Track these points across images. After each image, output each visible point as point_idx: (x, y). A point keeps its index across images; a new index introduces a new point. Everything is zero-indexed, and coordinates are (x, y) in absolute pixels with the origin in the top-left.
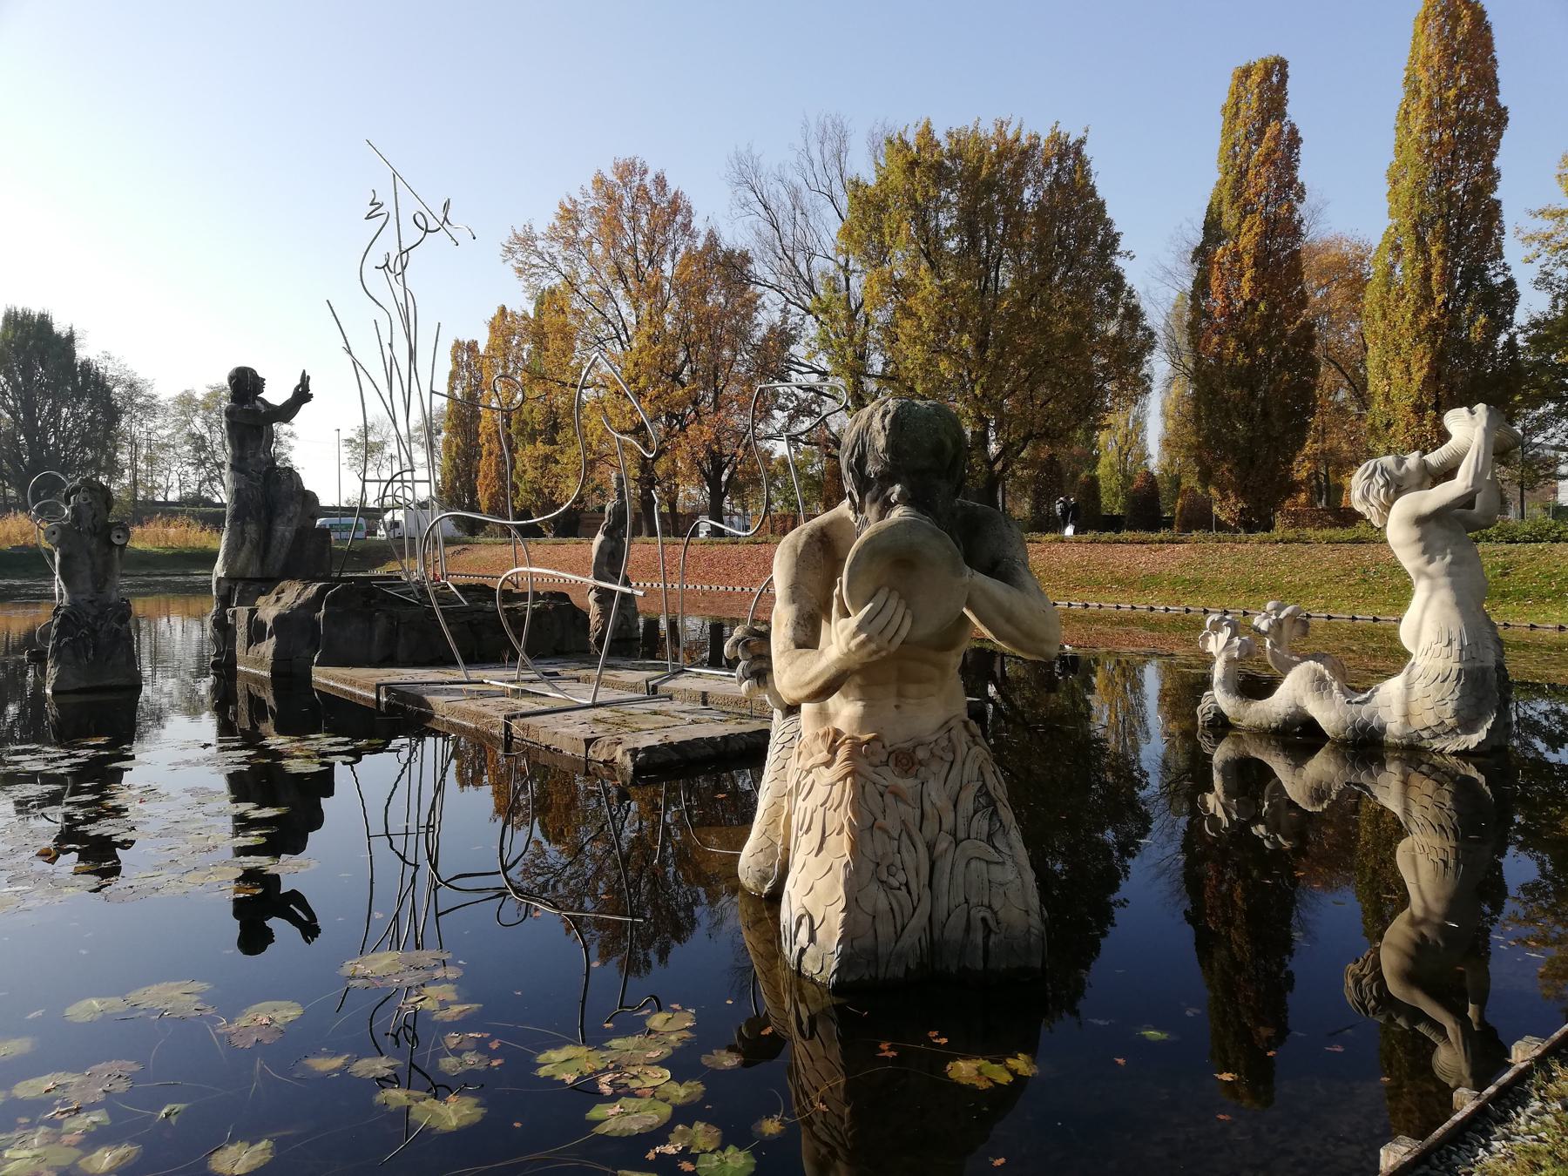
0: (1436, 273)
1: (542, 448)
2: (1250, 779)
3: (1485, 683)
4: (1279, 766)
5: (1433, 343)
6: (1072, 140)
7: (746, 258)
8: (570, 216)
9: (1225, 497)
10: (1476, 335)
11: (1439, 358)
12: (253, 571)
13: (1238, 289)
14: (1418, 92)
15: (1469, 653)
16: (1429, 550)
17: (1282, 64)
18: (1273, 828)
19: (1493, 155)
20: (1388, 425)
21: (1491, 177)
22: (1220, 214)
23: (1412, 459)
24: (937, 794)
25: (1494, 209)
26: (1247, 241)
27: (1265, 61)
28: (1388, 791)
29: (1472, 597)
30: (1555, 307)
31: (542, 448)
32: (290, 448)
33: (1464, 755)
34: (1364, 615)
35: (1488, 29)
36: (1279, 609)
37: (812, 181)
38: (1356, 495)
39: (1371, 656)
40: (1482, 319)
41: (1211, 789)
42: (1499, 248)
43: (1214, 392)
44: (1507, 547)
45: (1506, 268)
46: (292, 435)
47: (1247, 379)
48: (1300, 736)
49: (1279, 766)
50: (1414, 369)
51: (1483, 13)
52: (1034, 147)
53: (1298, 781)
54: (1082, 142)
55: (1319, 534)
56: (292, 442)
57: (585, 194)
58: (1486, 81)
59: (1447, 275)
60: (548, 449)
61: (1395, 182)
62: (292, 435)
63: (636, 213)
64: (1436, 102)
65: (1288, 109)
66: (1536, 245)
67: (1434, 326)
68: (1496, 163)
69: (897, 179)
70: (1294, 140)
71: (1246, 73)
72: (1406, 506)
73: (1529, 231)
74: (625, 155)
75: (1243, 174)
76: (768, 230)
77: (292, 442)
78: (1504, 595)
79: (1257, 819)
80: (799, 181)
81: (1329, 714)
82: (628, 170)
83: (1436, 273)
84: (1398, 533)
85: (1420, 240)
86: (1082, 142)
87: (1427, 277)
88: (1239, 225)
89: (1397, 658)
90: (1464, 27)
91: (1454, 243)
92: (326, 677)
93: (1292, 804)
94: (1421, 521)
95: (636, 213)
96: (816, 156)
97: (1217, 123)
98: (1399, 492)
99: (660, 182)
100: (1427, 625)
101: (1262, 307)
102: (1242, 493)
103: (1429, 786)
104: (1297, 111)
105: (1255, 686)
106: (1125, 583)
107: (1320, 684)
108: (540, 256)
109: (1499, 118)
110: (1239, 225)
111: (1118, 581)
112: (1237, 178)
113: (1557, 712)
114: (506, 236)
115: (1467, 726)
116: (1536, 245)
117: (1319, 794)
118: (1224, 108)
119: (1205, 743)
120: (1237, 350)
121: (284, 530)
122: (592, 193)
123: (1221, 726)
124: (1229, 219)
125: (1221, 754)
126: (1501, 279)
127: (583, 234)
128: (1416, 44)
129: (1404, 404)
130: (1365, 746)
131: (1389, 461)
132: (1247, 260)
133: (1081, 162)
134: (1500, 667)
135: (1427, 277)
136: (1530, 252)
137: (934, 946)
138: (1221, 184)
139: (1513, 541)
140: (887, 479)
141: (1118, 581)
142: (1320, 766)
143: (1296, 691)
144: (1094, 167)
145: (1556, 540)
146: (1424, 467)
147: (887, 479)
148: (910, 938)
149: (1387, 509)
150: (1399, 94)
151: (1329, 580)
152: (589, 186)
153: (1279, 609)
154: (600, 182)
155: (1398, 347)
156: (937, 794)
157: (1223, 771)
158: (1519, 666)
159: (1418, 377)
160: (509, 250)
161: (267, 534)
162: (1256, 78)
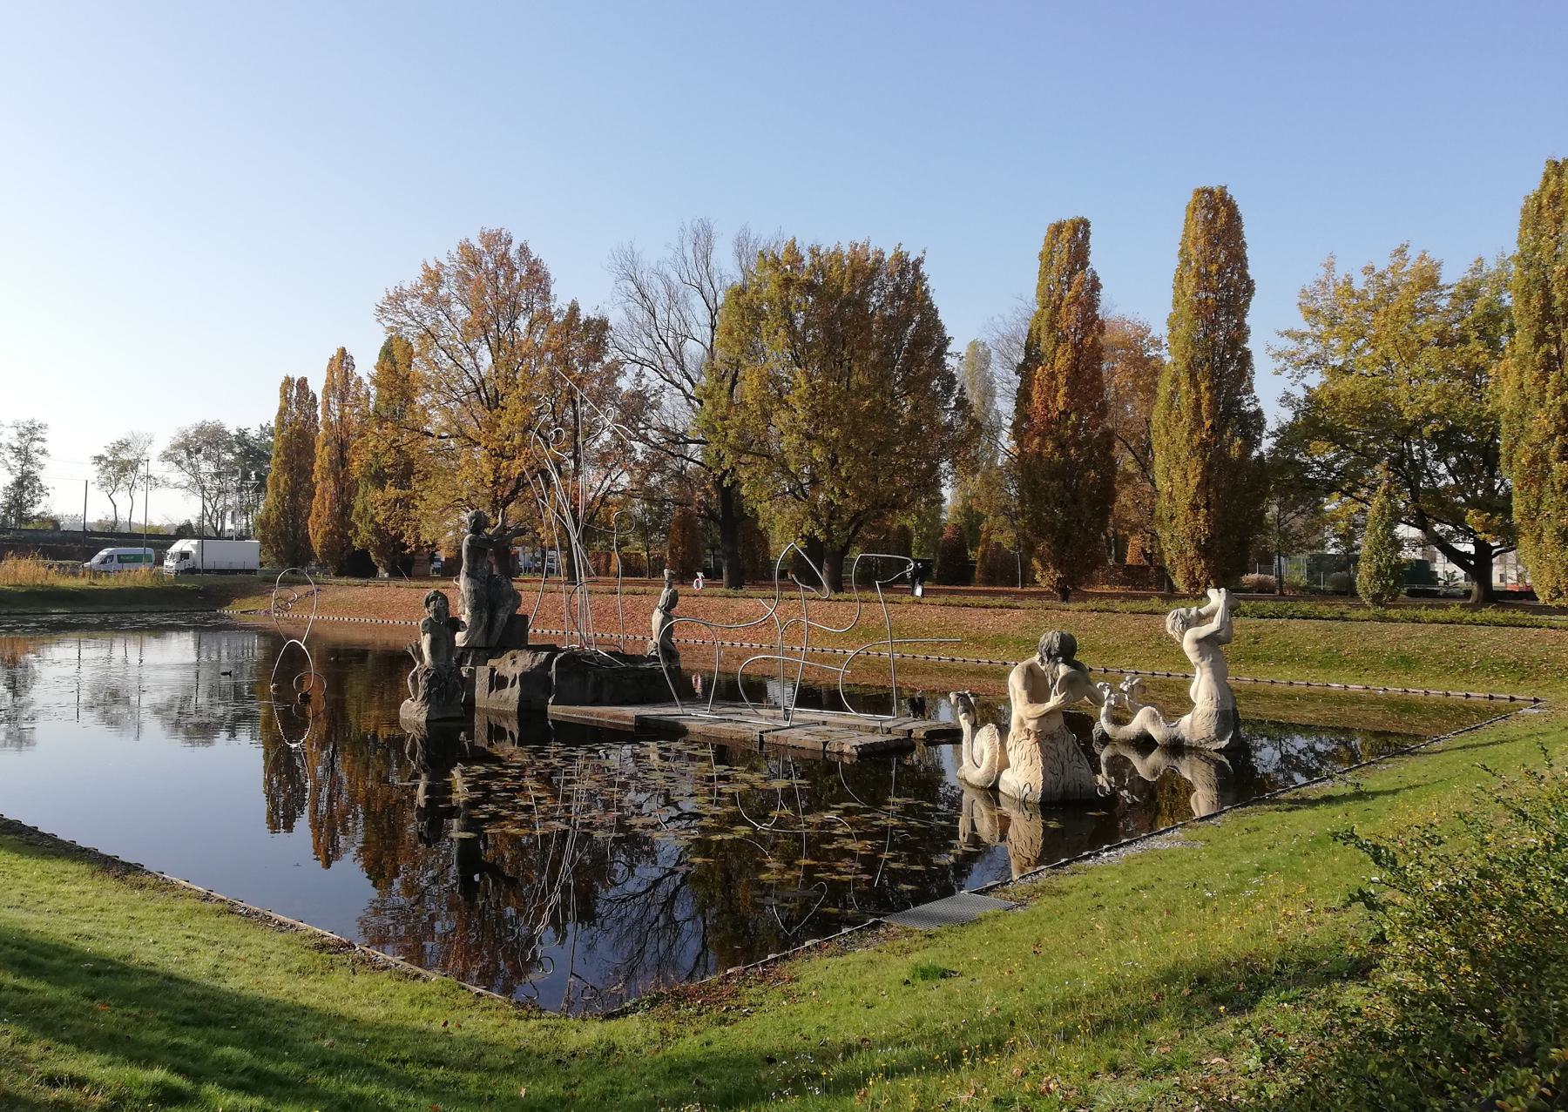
0: (1205, 403)
1: (392, 492)
2: (1119, 766)
3: (1227, 718)
4: (1135, 759)
5: (1204, 457)
6: (912, 258)
7: (600, 327)
8: (434, 277)
9: (1045, 567)
10: (1235, 453)
11: (1208, 468)
12: (482, 643)
13: (1054, 401)
14: (1188, 262)
15: (1220, 703)
16: (1202, 655)
17: (1086, 224)
18: (1132, 792)
19: (1244, 315)
20: (1172, 518)
21: (1242, 332)
22: (1039, 339)
23: (1194, 611)
24: (1062, 748)
25: (1245, 359)
26: (1061, 363)
27: (1072, 222)
28: (1188, 770)
29: (1219, 677)
30: (1296, 418)
31: (392, 492)
32: (41, 467)
33: (1219, 751)
34: (1161, 671)
35: (1239, 218)
36: (1132, 679)
37: (686, 278)
38: (1169, 626)
39: (1175, 702)
40: (1239, 441)
41: (1100, 772)
42: (1251, 385)
43: (1035, 482)
44: (1258, 621)
45: (1257, 400)
46: (44, 452)
47: (1063, 472)
48: (1144, 744)
49: (1135, 759)
50: (1190, 476)
51: (1235, 207)
52: (878, 261)
53: (1144, 766)
54: (919, 261)
55: (1124, 607)
56: (42, 459)
57: (451, 259)
58: (1238, 258)
59: (1213, 403)
60: (401, 493)
61: (1173, 329)
62: (44, 452)
63: (500, 282)
64: (1203, 270)
65: (1090, 259)
66: (1283, 361)
67: (1204, 445)
68: (1247, 321)
69: (771, 289)
70: (1095, 285)
71: (1058, 229)
72: (1191, 634)
73: (1277, 349)
74: (493, 226)
75: (1057, 308)
76: (642, 315)
77: (42, 459)
78: (1255, 658)
79: (1123, 788)
80: (674, 277)
81: (1158, 733)
82: (494, 239)
83: (1205, 403)
84: (1188, 646)
85: (1193, 376)
86: (919, 261)
87: (1198, 405)
88: (1055, 350)
89: (1187, 705)
90: (1221, 221)
91: (1217, 374)
92: (555, 710)
93: (1140, 779)
94: (1198, 641)
95: (500, 282)
96: (689, 254)
97: (1035, 266)
98: (1189, 627)
99: (524, 250)
100: (1202, 689)
101: (1073, 417)
102: (1059, 565)
103: (1205, 765)
104: (1098, 260)
105: (1119, 720)
106: (978, 641)
107: (1154, 717)
108: (409, 314)
109: (1250, 288)
110: (1055, 350)
111: (973, 639)
112: (1052, 305)
113: (1312, 749)
114: (380, 297)
115: (1220, 737)
116: (1283, 361)
117: (1154, 772)
118: (1041, 255)
119: (1097, 750)
120: (1055, 449)
121: (502, 616)
122: (457, 257)
123: (1105, 739)
124: (1046, 345)
125: (1104, 754)
126: (1252, 408)
127: (443, 292)
128: (1187, 228)
129: (1183, 503)
130: (1176, 748)
131: (1183, 610)
132: (1061, 379)
133: (919, 277)
134: (1235, 710)
135: (1198, 405)
136: (1279, 365)
137: (1065, 793)
138: (1039, 316)
139: (1262, 617)
140: (1057, 655)
141: (973, 639)
142: (1155, 758)
143: (1141, 721)
144: (931, 283)
145: (1292, 617)
146: (1199, 614)
147: (1057, 655)
148: (1060, 789)
149: (1182, 634)
150: (1175, 263)
151: (1134, 644)
152: (454, 250)
153: (1132, 679)
154: (465, 248)
155: (1178, 458)
156: (1062, 748)
157: (1107, 765)
158: (1246, 710)
159: (1193, 482)
160: (382, 310)
161: (492, 618)
162: (1066, 235)
